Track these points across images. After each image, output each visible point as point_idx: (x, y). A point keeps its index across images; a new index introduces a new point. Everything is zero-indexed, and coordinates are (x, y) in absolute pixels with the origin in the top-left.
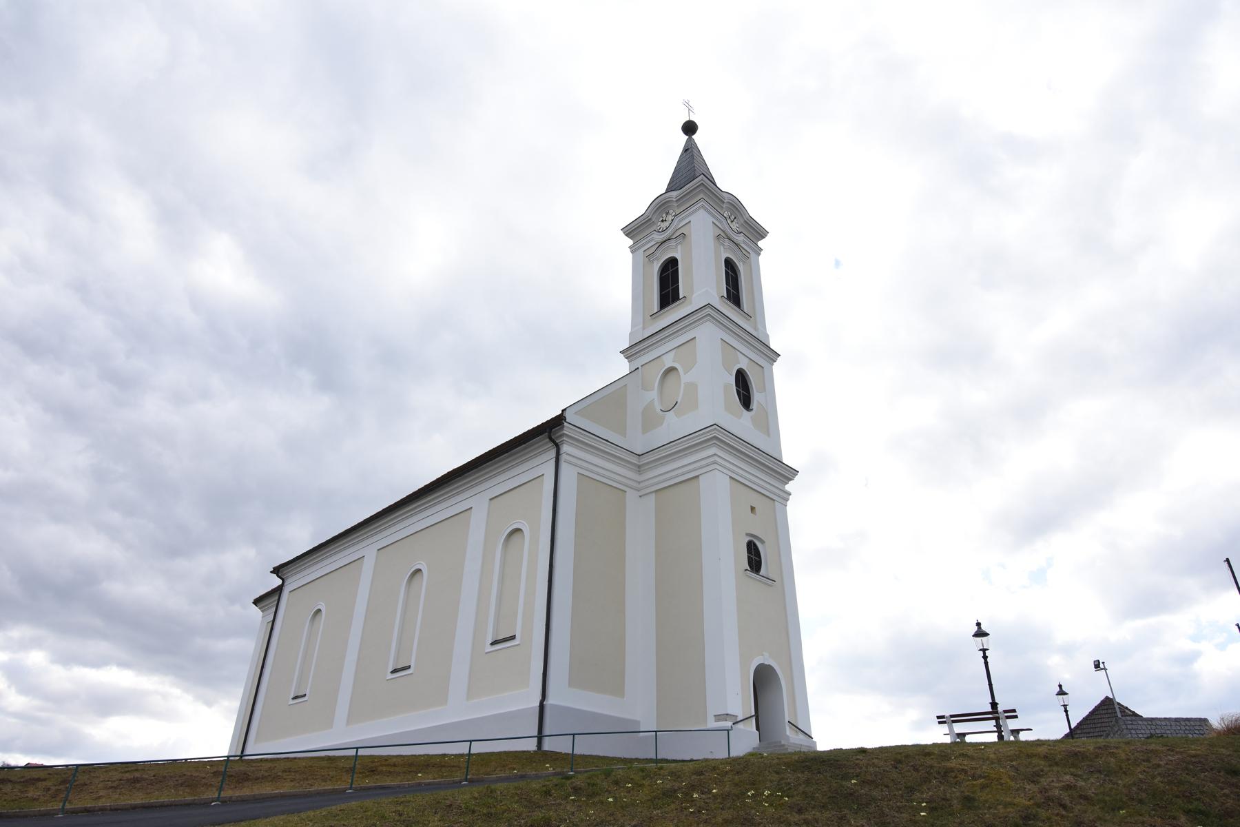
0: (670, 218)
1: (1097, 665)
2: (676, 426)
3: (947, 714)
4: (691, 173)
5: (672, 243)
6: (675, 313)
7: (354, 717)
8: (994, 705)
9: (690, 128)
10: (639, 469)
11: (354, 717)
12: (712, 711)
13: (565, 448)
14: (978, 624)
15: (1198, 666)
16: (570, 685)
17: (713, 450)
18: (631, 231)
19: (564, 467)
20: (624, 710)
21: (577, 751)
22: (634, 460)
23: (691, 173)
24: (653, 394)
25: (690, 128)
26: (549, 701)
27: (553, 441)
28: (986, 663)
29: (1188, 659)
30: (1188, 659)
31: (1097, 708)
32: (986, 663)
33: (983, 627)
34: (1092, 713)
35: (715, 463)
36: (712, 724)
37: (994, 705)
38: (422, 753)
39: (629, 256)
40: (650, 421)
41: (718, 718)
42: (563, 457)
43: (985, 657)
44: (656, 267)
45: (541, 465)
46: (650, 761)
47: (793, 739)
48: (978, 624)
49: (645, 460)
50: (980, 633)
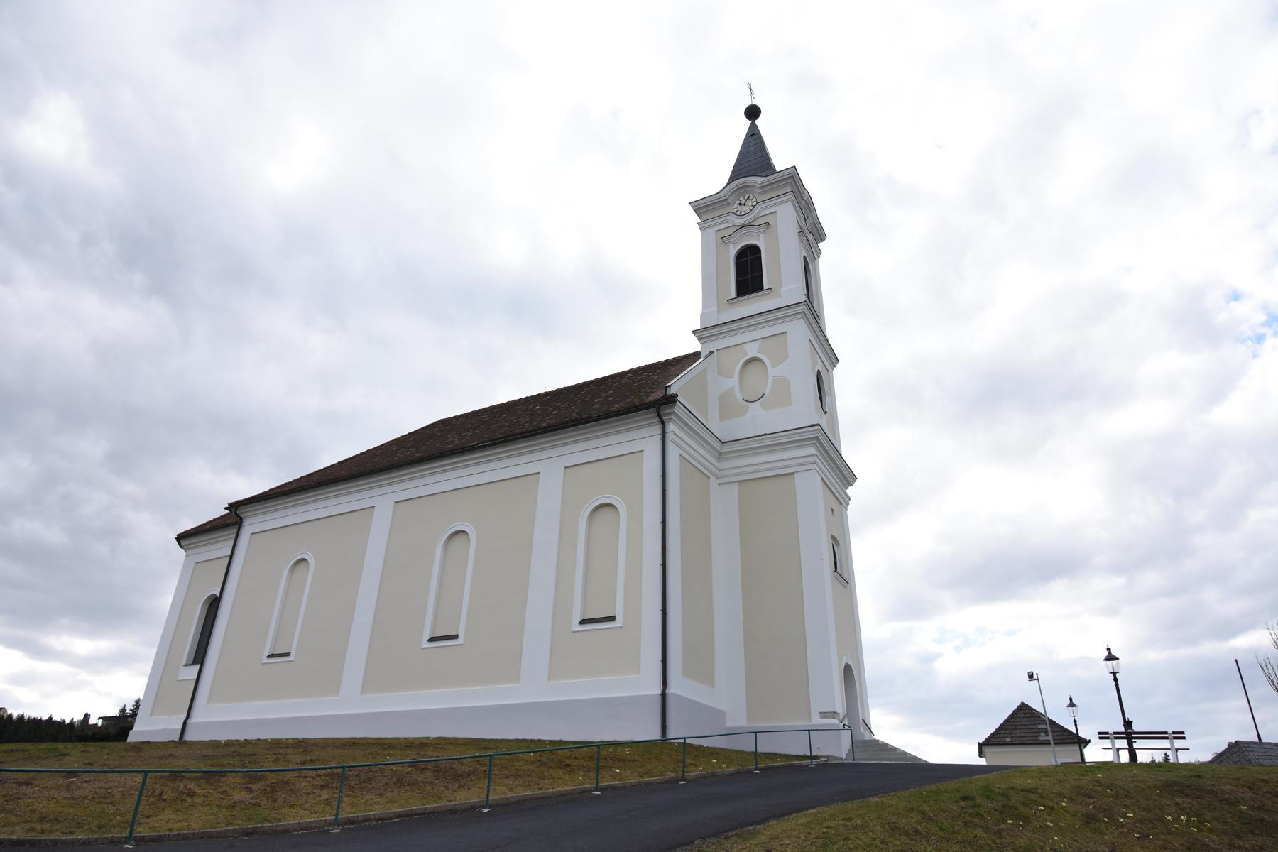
0: (749, 203)
1: (1031, 676)
2: (759, 420)
3: (1111, 731)
4: (754, 158)
5: (755, 230)
6: (754, 304)
7: (370, 684)
8: (1128, 724)
9: (753, 112)
10: (720, 456)
11: (370, 684)
12: (816, 709)
13: (671, 427)
14: (1109, 649)
15: (938, 664)
16: (1023, 704)
17: (812, 451)
18: (703, 208)
19: (671, 448)
20: (722, 705)
21: (762, 749)
22: (717, 445)
23: (754, 158)
24: (733, 382)
25: (753, 112)
26: (671, 690)
27: (659, 416)
28: (1117, 685)
29: (929, 659)
30: (929, 659)
31: (1015, 712)
32: (1117, 685)
33: (1113, 653)
34: (1011, 716)
35: (815, 463)
36: (816, 720)
37: (1128, 724)
38: (710, 745)
39: (697, 233)
40: (728, 408)
41: (824, 715)
42: (670, 437)
43: (1116, 680)
44: (733, 251)
45: (636, 443)
46: (805, 757)
47: (867, 737)
48: (1109, 649)
49: (728, 448)
50: (1110, 657)
